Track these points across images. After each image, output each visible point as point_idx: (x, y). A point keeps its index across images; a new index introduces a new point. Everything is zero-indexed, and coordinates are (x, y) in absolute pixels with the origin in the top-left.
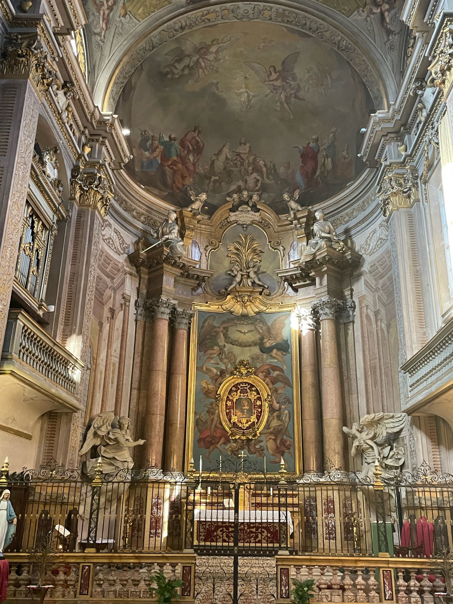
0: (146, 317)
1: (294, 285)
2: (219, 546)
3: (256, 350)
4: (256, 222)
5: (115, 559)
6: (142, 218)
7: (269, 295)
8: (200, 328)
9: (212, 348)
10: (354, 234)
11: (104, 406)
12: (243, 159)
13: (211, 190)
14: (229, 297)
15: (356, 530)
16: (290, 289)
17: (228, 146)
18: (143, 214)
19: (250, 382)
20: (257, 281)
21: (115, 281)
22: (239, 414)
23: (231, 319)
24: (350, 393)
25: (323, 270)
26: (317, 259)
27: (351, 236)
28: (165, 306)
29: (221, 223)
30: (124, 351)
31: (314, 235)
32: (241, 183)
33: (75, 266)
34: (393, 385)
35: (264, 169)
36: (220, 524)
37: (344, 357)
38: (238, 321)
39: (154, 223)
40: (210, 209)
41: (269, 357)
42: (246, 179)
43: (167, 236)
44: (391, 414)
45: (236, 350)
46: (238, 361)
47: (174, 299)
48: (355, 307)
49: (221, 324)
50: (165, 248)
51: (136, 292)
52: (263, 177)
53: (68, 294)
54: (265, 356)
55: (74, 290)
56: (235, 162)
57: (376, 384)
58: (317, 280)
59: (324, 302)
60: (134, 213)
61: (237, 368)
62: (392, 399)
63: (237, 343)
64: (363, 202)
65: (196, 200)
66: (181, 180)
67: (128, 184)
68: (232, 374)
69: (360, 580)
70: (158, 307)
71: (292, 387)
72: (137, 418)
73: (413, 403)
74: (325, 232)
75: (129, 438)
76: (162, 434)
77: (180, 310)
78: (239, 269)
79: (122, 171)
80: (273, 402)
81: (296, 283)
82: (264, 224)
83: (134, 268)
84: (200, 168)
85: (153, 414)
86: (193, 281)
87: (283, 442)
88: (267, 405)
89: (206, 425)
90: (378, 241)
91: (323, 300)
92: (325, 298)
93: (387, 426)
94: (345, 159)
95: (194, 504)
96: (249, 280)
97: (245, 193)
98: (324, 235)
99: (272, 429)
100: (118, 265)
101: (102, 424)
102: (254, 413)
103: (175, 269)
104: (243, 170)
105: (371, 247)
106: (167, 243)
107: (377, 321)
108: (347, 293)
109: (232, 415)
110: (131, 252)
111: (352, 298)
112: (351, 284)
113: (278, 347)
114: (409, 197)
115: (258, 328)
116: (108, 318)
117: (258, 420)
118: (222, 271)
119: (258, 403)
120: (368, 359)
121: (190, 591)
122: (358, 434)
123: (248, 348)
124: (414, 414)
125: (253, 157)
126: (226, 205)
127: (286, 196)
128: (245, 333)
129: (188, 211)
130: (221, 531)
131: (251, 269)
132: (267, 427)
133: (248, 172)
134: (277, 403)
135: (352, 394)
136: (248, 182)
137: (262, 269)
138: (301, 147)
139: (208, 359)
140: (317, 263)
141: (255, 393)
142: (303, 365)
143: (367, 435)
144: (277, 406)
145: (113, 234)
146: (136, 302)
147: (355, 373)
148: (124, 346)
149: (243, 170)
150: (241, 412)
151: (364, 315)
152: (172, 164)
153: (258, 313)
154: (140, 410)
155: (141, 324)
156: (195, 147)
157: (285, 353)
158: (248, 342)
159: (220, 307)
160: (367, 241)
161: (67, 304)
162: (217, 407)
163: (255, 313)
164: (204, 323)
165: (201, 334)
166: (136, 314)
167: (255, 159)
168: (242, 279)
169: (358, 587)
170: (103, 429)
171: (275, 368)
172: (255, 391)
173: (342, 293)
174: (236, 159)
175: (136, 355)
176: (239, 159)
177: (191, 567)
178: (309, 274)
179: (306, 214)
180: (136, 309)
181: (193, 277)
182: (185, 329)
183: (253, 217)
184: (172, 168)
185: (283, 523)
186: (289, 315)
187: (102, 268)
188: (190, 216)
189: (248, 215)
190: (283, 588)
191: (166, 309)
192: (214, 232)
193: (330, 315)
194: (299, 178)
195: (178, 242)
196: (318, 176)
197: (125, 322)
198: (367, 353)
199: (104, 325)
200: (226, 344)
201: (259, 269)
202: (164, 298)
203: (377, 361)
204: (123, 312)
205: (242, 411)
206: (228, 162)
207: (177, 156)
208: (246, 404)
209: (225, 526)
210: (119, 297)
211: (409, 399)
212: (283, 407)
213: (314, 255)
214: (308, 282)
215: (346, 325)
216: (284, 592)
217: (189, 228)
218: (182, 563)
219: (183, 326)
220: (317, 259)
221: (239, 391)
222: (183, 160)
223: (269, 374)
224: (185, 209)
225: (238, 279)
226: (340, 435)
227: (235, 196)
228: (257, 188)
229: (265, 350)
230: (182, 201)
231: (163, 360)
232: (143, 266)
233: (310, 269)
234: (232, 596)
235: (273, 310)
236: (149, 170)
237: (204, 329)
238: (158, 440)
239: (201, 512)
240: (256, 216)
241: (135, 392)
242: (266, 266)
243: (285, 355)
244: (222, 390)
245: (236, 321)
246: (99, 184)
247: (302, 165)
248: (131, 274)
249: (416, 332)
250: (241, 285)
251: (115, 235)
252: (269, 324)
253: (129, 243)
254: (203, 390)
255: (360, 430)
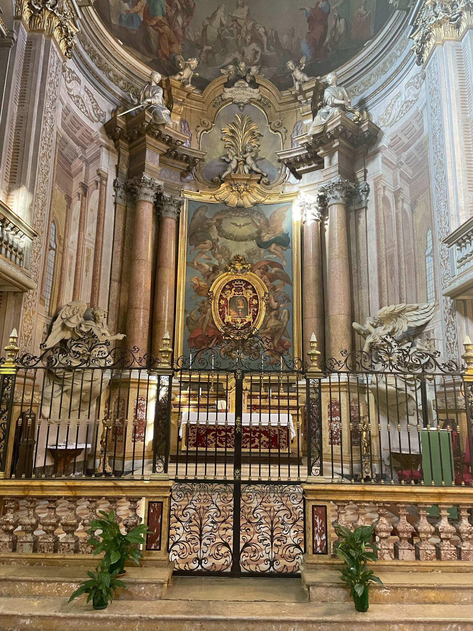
0: (127, 200)
1: (297, 170)
2: (210, 452)
3: (252, 245)
4: (254, 100)
5: (34, 490)
6: (121, 83)
7: (268, 184)
8: (191, 219)
9: (203, 241)
10: (371, 105)
11: (77, 296)
12: (240, 26)
13: (203, 62)
14: (223, 185)
15: (366, 435)
16: (292, 175)
17: (223, 9)
18: (122, 78)
19: (246, 279)
20: (255, 168)
21: (87, 151)
22: (233, 313)
23: (225, 210)
24: (359, 288)
25: (335, 146)
26: (327, 131)
27: (366, 108)
28: (148, 186)
29: (214, 100)
30: (101, 236)
31: (324, 105)
32: (237, 55)
33: (24, 108)
34: (416, 274)
35: (265, 38)
36: (212, 428)
37: (353, 248)
38: (233, 212)
39: (136, 92)
40: (201, 83)
41: (267, 252)
42: (243, 50)
43: (149, 100)
44: (416, 305)
45: (231, 244)
46: (232, 256)
47: (159, 179)
48: (368, 191)
49: (214, 216)
50: (146, 113)
51: (114, 170)
52: (262, 49)
53: (14, 143)
54: (262, 251)
55: (22, 138)
56: (231, 29)
57: (392, 275)
58: (326, 160)
59: (333, 183)
60: (111, 75)
61: (231, 264)
62: (414, 289)
63: (231, 237)
64: (385, 63)
65: (186, 66)
66: (168, 46)
67: (102, 34)
68: (226, 270)
69: (444, 524)
70: (141, 187)
71: (292, 285)
72: (119, 312)
73: (463, 283)
74: (338, 99)
75: (106, 332)
76: (146, 330)
77: (166, 195)
78: (234, 154)
79: (90, 7)
80: (270, 301)
81: (299, 168)
82: (263, 103)
83: (112, 141)
84: (190, 34)
85: (135, 308)
86: (182, 164)
87: (281, 343)
88: (264, 304)
89: (198, 324)
90: (402, 106)
91: (333, 182)
92: (336, 179)
93: (409, 319)
94: (361, 16)
95: (180, 405)
96: (245, 167)
97: (243, 65)
98: (337, 101)
99: (269, 329)
100: (91, 134)
101: (72, 315)
102: (250, 313)
103: (160, 143)
104: (240, 39)
105: (392, 116)
106: (150, 108)
107: (397, 202)
108: (360, 175)
109: (226, 315)
110: (107, 120)
111: (365, 180)
112: (365, 165)
113: (278, 241)
114: (458, 26)
115: (255, 221)
116: (79, 194)
117: (254, 319)
118: (215, 157)
119: (255, 302)
120: (383, 248)
121: (160, 543)
122: (372, 330)
123: (244, 243)
124: (460, 298)
125: (251, 23)
126: (220, 78)
127: (290, 64)
128: (240, 226)
129: (175, 80)
130: (213, 435)
131: (248, 154)
132: (264, 326)
133: (246, 42)
134: (275, 302)
135: (361, 289)
136: (246, 54)
137: (260, 155)
138: (308, 9)
139: (200, 254)
140: (327, 137)
141: (251, 291)
142: (305, 259)
143: (384, 329)
144: (274, 304)
145: (83, 92)
146: (115, 181)
147: (366, 265)
148: (101, 231)
149: (240, 39)
150: (236, 311)
151: (380, 199)
152: (157, 25)
153: (255, 204)
154: (121, 304)
155: (121, 209)
156: (184, 6)
157: (284, 248)
158: (244, 236)
159: (213, 197)
160: (387, 110)
161: (13, 156)
162: (209, 306)
163: (252, 204)
164: (195, 213)
165: (191, 226)
166: (115, 196)
167: (253, 26)
168: (237, 166)
169: (443, 536)
170: (73, 320)
171: (273, 264)
172: (251, 289)
173: (354, 174)
174: (232, 26)
175: (116, 243)
176: (235, 25)
177: (162, 502)
178: (316, 153)
179: (314, 85)
180: (115, 190)
181: (181, 159)
182: (173, 218)
183: (251, 94)
184: (157, 30)
185: (284, 427)
186: (291, 205)
187: (68, 130)
188: (178, 86)
189: (245, 92)
190: (317, 537)
191: (150, 190)
192: (207, 111)
193: (341, 199)
194: (304, 47)
195: (163, 109)
196: (327, 43)
197: (101, 203)
198: (382, 241)
199: (74, 201)
200: (219, 238)
201: (257, 155)
202: (147, 176)
203: (396, 248)
204: (98, 191)
205: (237, 311)
206: (223, 28)
207: (163, 15)
208: (241, 303)
209: (216, 430)
210: (92, 173)
211: (456, 277)
212: (281, 305)
213: (325, 126)
214: (314, 165)
215: (357, 212)
216: (319, 544)
217: (177, 102)
218: (147, 497)
219: (171, 215)
220: (327, 131)
221: (234, 289)
222: (171, 22)
223: (267, 270)
224: (173, 77)
225: (233, 165)
226: (348, 333)
227: (231, 67)
228: (256, 61)
229: (262, 245)
230: (169, 69)
231: (147, 249)
232: (122, 139)
233: (318, 147)
234: (231, 547)
235: (273, 200)
236: (129, 28)
237: (195, 221)
238: (141, 336)
239: (189, 415)
240: (255, 93)
241: (115, 285)
242: (266, 152)
243: (285, 250)
244: (216, 288)
245: (230, 213)
246: (56, 5)
247: (309, 31)
248: (108, 148)
249: (465, 197)
250: (237, 173)
251: (86, 95)
252: (268, 216)
253: (105, 110)
254: (193, 287)
255: (375, 324)
